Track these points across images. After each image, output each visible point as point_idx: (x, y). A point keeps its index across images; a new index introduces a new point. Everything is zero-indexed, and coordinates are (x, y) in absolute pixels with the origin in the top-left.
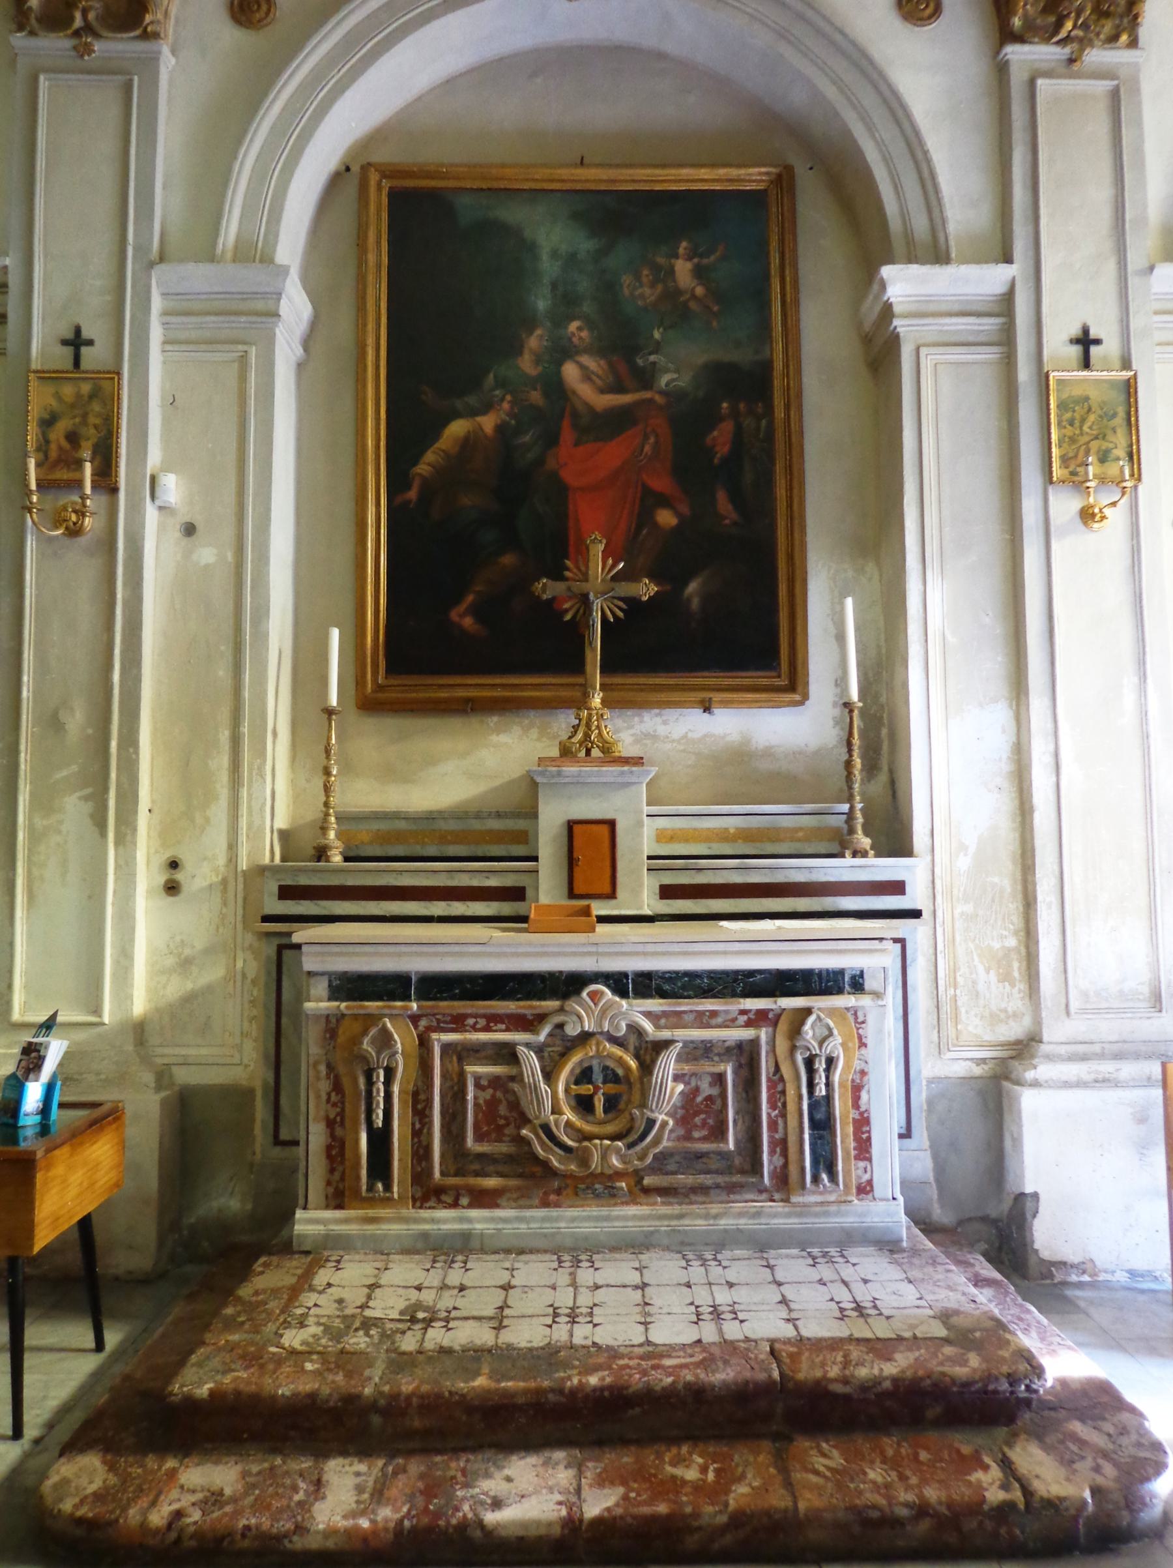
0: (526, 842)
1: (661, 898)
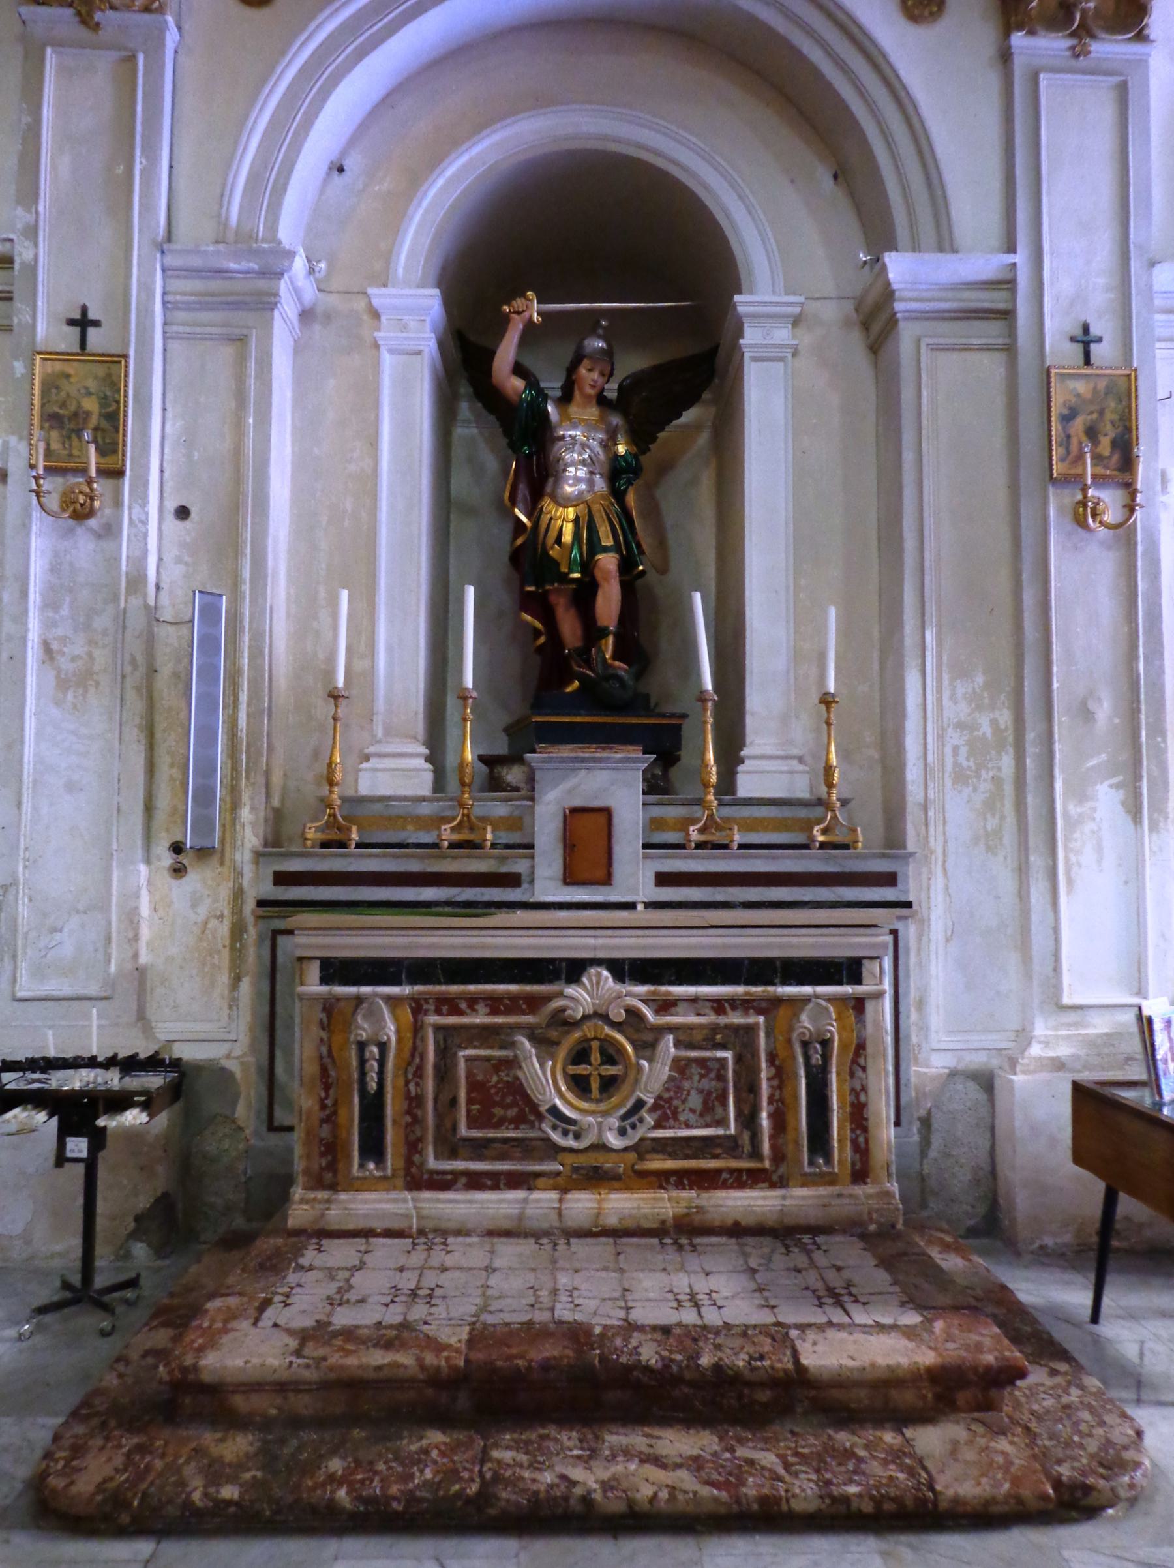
0: (520, 829)
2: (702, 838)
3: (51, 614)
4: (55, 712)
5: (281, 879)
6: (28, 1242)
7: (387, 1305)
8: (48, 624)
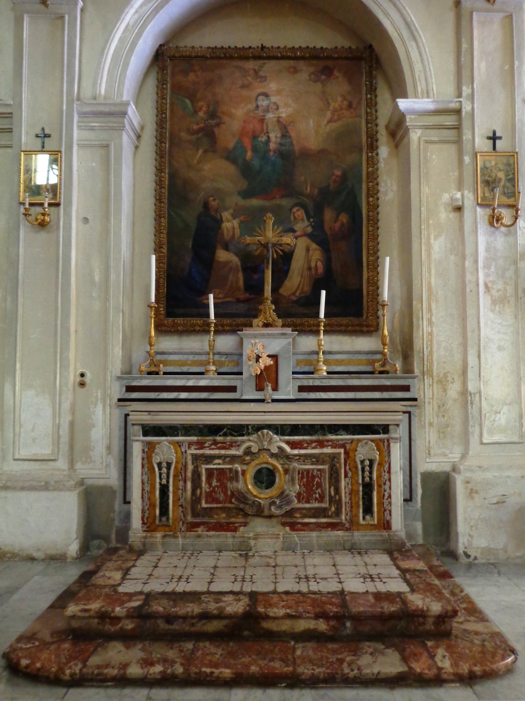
1: (236, 392)
2: (382, 369)
3: (487, 271)
4: (492, 315)
5: (130, 389)
6: (506, 552)
7: (233, 582)
8: (487, 275)
